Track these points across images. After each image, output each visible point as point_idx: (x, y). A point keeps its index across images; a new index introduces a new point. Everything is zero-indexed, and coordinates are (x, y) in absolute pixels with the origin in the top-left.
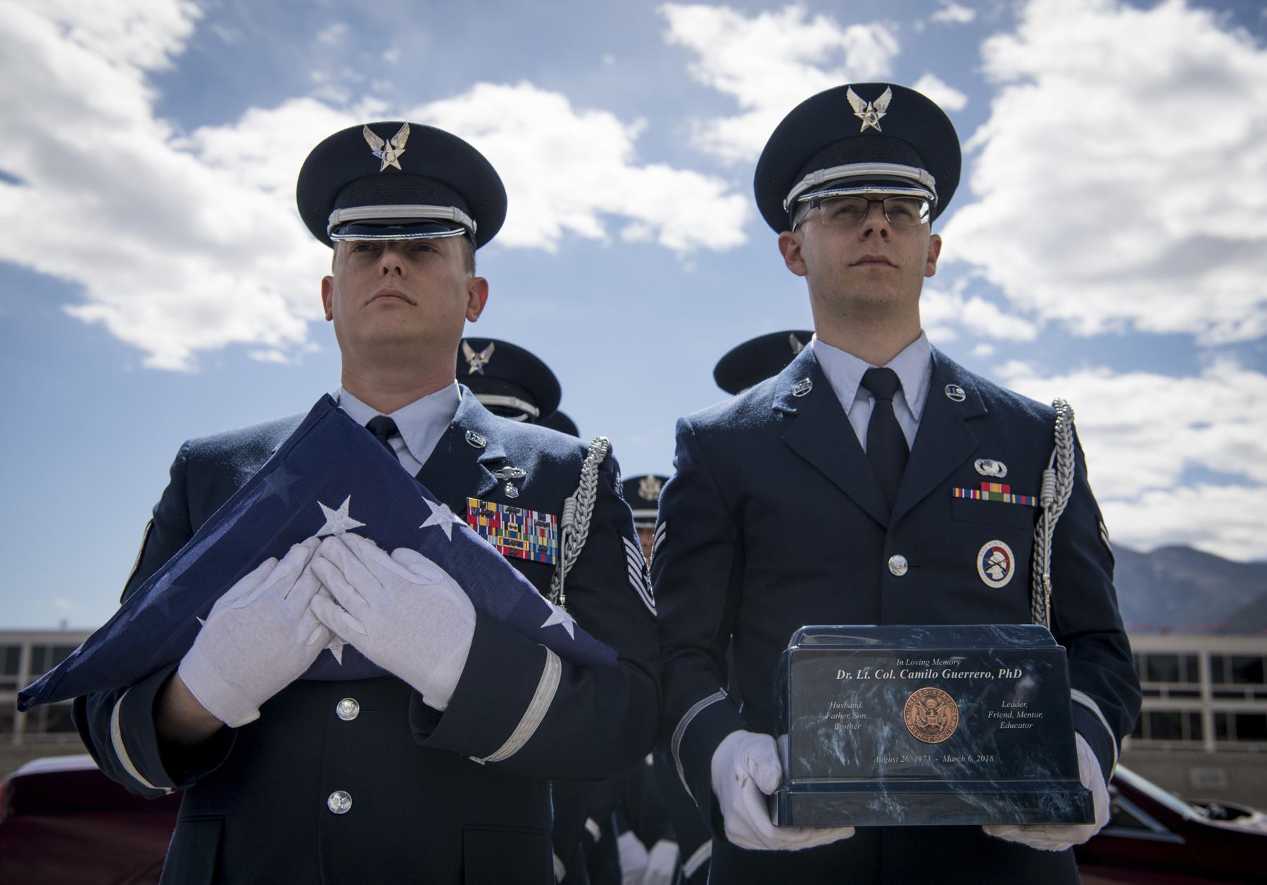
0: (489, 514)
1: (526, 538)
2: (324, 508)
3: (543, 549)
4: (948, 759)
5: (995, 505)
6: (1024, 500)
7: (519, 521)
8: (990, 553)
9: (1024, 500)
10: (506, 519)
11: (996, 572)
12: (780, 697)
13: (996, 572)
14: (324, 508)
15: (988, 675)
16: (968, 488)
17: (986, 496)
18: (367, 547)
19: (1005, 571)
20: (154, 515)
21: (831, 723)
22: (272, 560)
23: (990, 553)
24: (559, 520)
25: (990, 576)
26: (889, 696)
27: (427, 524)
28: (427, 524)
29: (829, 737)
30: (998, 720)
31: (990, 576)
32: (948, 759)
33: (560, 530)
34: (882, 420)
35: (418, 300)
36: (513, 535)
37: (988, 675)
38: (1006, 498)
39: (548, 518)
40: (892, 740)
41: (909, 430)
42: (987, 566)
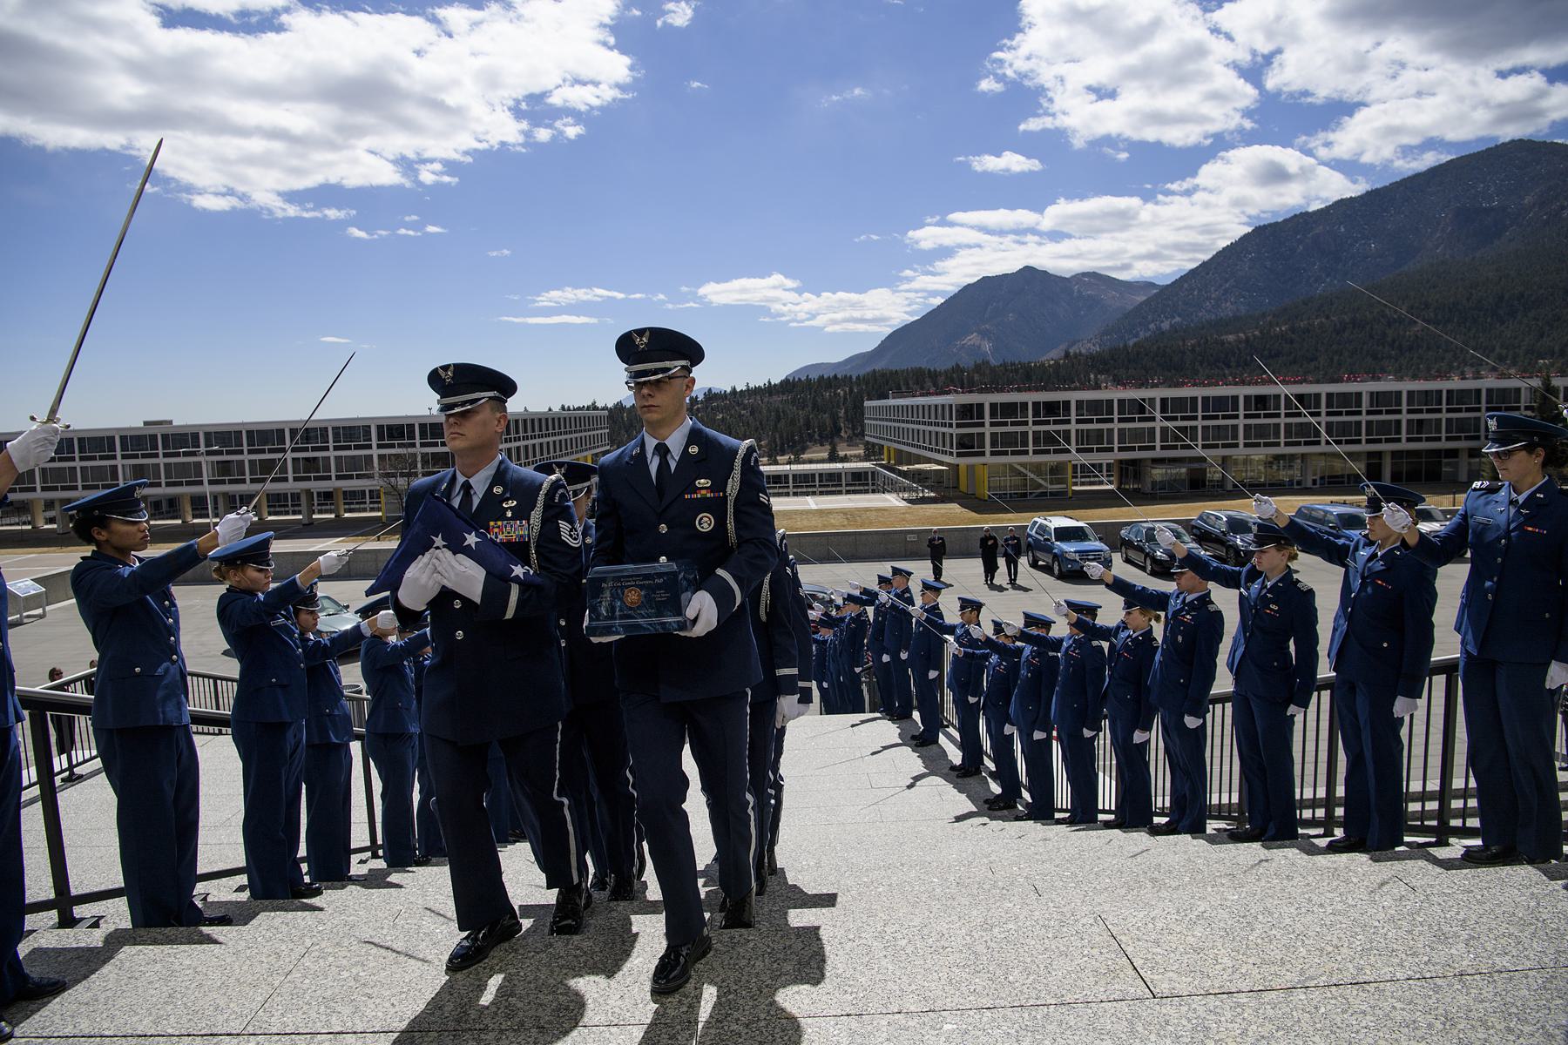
0: (499, 527)
1: (514, 533)
2: (434, 538)
3: (522, 536)
4: (638, 612)
5: (704, 499)
6: (717, 495)
7: (511, 526)
8: (701, 519)
9: (717, 495)
10: (506, 527)
11: (705, 525)
12: (1442, 246)
13: (705, 525)
14: (434, 538)
15: (652, 582)
16: (691, 494)
17: (699, 496)
18: (448, 553)
19: (710, 525)
20: (623, 52)
21: (601, 602)
22: (420, 556)
23: (701, 519)
24: (528, 523)
25: (702, 528)
26: (619, 592)
27: (465, 544)
28: (465, 544)
29: (600, 606)
30: (655, 598)
31: (702, 528)
32: (638, 612)
33: (529, 525)
34: (663, 465)
35: (466, 433)
36: (509, 533)
37: (652, 582)
38: (708, 495)
39: (524, 522)
40: (620, 607)
41: (673, 466)
42: (700, 524)
